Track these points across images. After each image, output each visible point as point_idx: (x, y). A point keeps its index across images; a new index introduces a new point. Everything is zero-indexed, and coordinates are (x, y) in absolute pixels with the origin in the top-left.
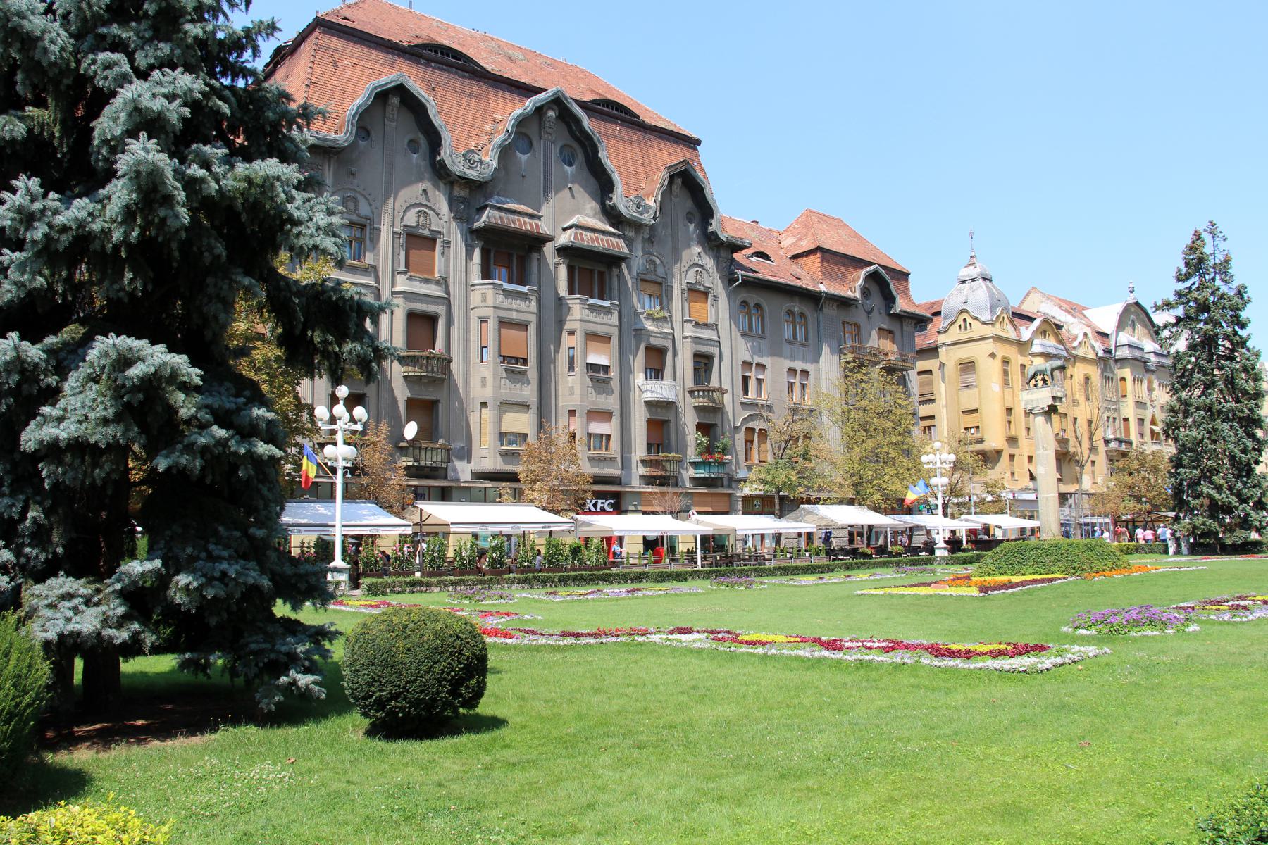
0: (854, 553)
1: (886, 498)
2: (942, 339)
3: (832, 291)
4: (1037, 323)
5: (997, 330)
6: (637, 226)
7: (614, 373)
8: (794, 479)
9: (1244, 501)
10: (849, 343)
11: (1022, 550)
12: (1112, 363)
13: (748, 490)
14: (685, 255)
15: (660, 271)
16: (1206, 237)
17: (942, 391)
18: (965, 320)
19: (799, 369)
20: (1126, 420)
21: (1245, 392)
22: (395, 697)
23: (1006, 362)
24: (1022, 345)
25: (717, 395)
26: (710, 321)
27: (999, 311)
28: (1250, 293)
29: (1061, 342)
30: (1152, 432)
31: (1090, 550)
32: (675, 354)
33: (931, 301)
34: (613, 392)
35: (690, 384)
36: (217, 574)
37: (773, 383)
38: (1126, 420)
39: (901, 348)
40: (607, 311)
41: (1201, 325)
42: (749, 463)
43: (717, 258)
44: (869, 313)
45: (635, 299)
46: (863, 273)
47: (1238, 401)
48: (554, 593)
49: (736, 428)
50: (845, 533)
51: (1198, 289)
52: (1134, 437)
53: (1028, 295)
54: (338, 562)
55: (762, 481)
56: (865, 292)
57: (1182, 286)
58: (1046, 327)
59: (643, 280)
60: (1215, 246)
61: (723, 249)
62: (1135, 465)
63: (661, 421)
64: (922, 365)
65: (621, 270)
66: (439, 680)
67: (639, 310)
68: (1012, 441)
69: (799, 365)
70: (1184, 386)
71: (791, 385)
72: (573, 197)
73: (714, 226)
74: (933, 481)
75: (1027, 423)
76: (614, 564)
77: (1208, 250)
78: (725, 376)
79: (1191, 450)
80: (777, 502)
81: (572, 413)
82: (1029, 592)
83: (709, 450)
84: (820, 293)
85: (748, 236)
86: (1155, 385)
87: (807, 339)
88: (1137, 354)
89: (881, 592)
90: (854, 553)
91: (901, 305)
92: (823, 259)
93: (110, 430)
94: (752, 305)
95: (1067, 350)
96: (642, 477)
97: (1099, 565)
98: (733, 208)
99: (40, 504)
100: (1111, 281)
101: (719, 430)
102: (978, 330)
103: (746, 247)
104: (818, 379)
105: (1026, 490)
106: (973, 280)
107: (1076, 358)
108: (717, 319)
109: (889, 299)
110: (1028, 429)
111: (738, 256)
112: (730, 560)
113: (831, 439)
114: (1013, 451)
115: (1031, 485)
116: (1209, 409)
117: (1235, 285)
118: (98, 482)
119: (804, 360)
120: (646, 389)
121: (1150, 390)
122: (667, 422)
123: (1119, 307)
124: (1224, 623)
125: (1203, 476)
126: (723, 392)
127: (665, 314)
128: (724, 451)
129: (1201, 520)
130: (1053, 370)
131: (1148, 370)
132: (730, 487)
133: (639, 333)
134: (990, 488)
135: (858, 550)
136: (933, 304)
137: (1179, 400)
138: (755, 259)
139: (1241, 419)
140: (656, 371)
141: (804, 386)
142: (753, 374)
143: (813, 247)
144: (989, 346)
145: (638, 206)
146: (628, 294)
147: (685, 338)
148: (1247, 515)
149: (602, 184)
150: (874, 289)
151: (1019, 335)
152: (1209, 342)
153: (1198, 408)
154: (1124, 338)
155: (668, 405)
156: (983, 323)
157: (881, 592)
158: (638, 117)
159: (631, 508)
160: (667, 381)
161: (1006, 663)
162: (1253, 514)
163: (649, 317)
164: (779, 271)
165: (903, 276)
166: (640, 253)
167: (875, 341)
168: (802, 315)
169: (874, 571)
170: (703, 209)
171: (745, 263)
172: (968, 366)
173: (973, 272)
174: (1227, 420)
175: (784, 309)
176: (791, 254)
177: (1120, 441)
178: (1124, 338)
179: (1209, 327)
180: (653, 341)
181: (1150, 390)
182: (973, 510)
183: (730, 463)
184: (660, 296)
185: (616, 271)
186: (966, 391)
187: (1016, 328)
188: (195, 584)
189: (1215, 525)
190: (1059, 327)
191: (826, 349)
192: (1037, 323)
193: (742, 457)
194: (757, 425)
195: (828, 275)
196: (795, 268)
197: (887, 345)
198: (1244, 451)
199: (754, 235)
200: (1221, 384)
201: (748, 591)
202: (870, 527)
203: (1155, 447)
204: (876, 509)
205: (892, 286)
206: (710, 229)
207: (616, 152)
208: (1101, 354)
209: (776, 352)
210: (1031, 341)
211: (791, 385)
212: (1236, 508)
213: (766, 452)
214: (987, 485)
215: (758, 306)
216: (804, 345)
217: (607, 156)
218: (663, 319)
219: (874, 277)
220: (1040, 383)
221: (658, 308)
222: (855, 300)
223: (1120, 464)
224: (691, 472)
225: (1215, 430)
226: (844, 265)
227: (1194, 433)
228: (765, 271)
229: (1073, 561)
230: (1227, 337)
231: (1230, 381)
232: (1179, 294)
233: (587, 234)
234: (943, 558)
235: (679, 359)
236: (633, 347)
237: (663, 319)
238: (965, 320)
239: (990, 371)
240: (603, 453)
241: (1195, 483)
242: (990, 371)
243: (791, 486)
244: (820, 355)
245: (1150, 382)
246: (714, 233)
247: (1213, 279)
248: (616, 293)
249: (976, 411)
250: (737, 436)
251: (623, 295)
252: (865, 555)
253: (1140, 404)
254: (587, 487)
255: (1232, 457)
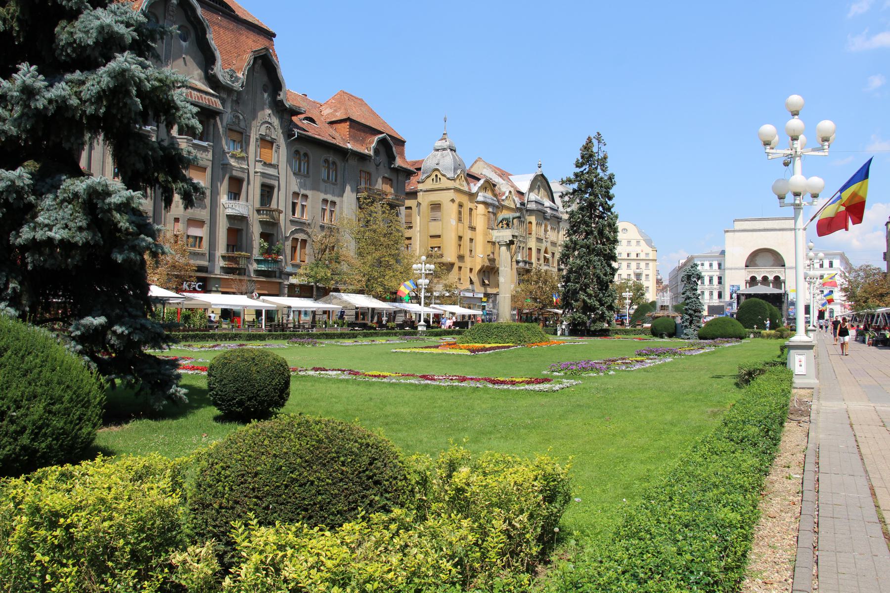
0: (364, 326)
1: (386, 290)
2: (420, 187)
3: (355, 149)
4: (482, 182)
5: (456, 184)
6: (229, 90)
7: (208, 193)
8: (329, 275)
9: (602, 305)
10: (363, 186)
11: (489, 328)
12: (524, 212)
13: (293, 280)
14: (260, 114)
15: (242, 124)
16: (595, 142)
17: (417, 221)
18: (436, 176)
19: (330, 200)
20: (530, 249)
21: (608, 239)
22: (250, 399)
23: (461, 206)
24: (472, 196)
25: (275, 214)
26: (274, 162)
27: (459, 172)
28: (616, 179)
29: (495, 195)
30: (545, 257)
31: (528, 330)
32: (248, 183)
33: (414, 160)
34: (206, 207)
35: (257, 205)
36: (138, 326)
37: (312, 209)
38: (530, 249)
39: (396, 191)
40: (205, 149)
41: (587, 196)
42: (293, 262)
43: (281, 119)
44: (377, 166)
45: (224, 142)
46: (376, 138)
47: (603, 244)
48: (189, 346)
49: (286, 238)
50: (354, 312)
51: (588, 173)
52: (534, 260)
53: (475, 162)
54: (422, 323)
55: (307, 275)
56: (376, 151)
57: (578, 170)
58: (487, 185)
59: (230, 129)
60: (599, 148)
61: (286, 113)
62: (535, 278)
63: (237, 228)
64: (408, 203)
65: (216, 121)
66: (275, 389)
67: (226, 150)
68: (461, 258)
69: (330, 197)
70: (575, 232)
71: (324, 210)
72: (185, 64)
73: (281, 97)
74: (420, 281)
75: (471, 247)
76: (211, 328)
77: (595, 149)
78: (281, 201)
79: (575, 272)
80: (315, 289)
81: (177, 220)
82: (499, 354)
83: (268, 251)
84: (348, 149)
85: (303, 106)
86: (549, 228)
87: (336, 180)
88: (540, 207)
89: (409, 351)
90: (364, 326)
91: (399, 162)
92: (351, 127)
93: (85, 234)
94: (302, 153)
95: (498, 201)
96: (222, 268)
97: (534, 340)
98: (296, 85)
99: (16, 278)
100: (532, 159)
101: (275, 238)
102: (444, 183)
103: (301, 113)
104: (341, 208)
105: (467, 290)
106: (444, 149)
107: (504, 207)
108: (278, 161)
109: (392, 158)
110: (471, 251)
111: (295, 119)
112: (283, 327)
113: (348, 247)
114: (461, 264)
115: (470, 287)
116: (588, 247)
117: (608, 173)
118: (70, 267)
119: (333, 194)
120: (228, 206)
121: (546, 231)
122: (241, 230)
123: (531, 176)
124: (623, 371)
125: (581, 289)
126: (280, 212)
127: (243, 154)
128: (279, 253)
129: (579, 314)
130: (514, 218)
131: (545, 219)
132: (280, 277)
133: (226, 167)
134: (448, 287)
135: (364, 324)
136: (416, 162)
137: (571, 240)
138: (305, 122)
139: (605, 255)
140: (235, 194)
141: (332, 212)
142: (299, 201)
143: (345, 117)
144: (451, 194)
145: (232, 76)
146: (220, 139)
147: (256, 172)
148: (603, 313)
149: (207, 59)
150: (382, 150)
151: (470, 189)
152: (591, 206)
153: (582, 247)
154: (533, 196)
155: (242, 219)
156: (448, 179)
157: (409, 351)
158: (234, 12)
159: (214, 289)
160: (242, 202)
161: (537, 387)
162: (607, 313)
163: (233, 156)
164: (320, 131)
165: (401, 143)
166: (229, 110)
167: (380, 185)
168: (334, 163)
169: (372, 338)
170: (274, 84)
171: (299, 124)
172: (436, 207)
173: (445, 144)
174: (597, 255)
175: (323, 158)
176: (329, 120)
177: (525, 262)
178: (533, 196)
179: (592, 197)
180: (235, 173)
181: (546, 231)
182: (433, 301)
183: (281, 261)
184: (241, 142)
185: (212, 121)
186: (433, 223)
187: (468, 184)
188: (127, 332)
189: (586, 318)
190: (494, 185)
191: (348, 188)
192: (482, 182)
193: (289, 258)
194: (301, 236)
195: (353, 138)
196: (331, 131)
197: (387, 188)
198: (605, 275)
199: (304, 104)
200: (596, 233)
201: (314, 348)
202: (373, 309)
203: (546, 268)
204: (378, 297)
205: (394, 149)
206: (279, 98)
207: (218, 36)
208: (518, 206)
209: (315, 188)
210: (476, 194)
211: (324, 210)
212: (598, 309)
213: (307, 256)
214: (446, 286)
215: (306, 155)
216: (334, 184)
217: (212, 38)
218: (242, 158)
219: (383, 142)
220: (505, 226)
221: (239, 150)
222: (370, 156)
223: (525, 277)
224: (255, 266)
225: (590, 261)
226: (364, 132)
227: (578, 262)
228: (313, 131)
229: (520, 336)
230: (601, 205)
231: (601, 233)
232: (576, 175)
233: (194, 93)
234: (423, 332)
235: (251, 187)
236: (221, 176)
237: (242, 158)
238: (436, 176)
239: (450, 211)
240: (197, 249)
241: (575, 292)
242: (450, 211)
243: (327, 280)
244: (344, 192)
245: (546, 226)
246: (281, 102)
247: (596, 168)
248: (211, 137)
249: (439, 236)
250: (287, 243)
251: (216, 139)
252: (371, 328)
253: (539, 240)
254: (193, 274)
255: (598, 278)
